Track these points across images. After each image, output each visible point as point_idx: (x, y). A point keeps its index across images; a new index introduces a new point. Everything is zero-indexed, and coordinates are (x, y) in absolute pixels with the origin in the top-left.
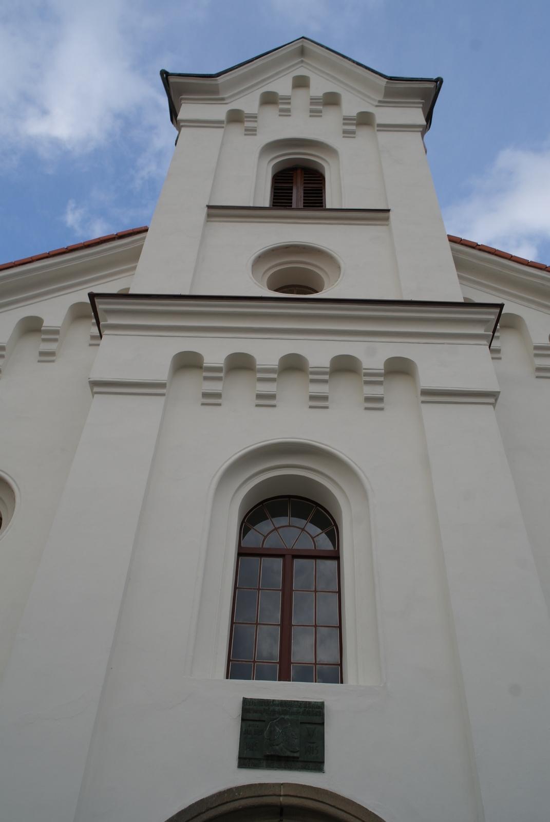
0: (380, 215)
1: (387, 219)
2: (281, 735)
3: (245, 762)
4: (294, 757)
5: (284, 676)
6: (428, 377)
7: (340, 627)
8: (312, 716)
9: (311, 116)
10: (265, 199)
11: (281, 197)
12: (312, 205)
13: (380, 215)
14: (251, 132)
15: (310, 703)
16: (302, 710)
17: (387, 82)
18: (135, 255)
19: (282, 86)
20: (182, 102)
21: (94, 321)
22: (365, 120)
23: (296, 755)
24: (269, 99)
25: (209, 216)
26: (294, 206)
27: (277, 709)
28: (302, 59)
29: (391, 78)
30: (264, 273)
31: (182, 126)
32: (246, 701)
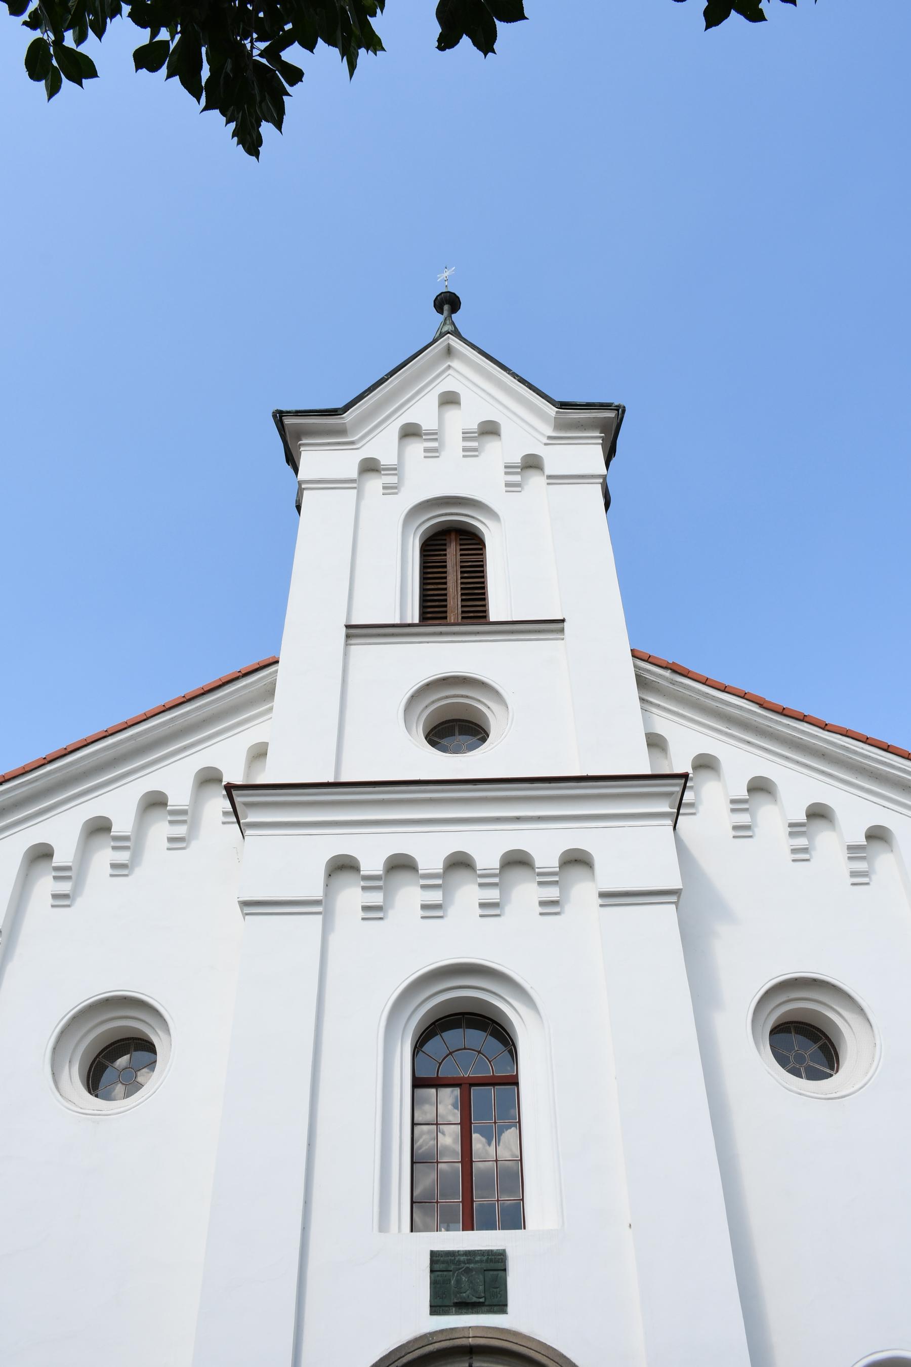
1: (562, 631)
2: (466, 1282)
3: (436, 1309)
5: (468, 1225)
6: (610, 874)
7: (521, 1160)
8: (494, 1265)
10: (413, 615)
11: (433, 611)
12: (472, 615)
14: (390, 489)
15: (492, 1251)
17: (557, 412)
18: (269, 693)
19: (423, 411)
20: (302, 449)
21: (235, 820)
22: (532, 464)
23: (482, 1300)
24: (410, 432)
25: (348, 636)
26: (452, 618)
27: (462, 1258)
28: (449, 363)
29: (563, 405)
30: (418, 527)
32: (433, 1253)
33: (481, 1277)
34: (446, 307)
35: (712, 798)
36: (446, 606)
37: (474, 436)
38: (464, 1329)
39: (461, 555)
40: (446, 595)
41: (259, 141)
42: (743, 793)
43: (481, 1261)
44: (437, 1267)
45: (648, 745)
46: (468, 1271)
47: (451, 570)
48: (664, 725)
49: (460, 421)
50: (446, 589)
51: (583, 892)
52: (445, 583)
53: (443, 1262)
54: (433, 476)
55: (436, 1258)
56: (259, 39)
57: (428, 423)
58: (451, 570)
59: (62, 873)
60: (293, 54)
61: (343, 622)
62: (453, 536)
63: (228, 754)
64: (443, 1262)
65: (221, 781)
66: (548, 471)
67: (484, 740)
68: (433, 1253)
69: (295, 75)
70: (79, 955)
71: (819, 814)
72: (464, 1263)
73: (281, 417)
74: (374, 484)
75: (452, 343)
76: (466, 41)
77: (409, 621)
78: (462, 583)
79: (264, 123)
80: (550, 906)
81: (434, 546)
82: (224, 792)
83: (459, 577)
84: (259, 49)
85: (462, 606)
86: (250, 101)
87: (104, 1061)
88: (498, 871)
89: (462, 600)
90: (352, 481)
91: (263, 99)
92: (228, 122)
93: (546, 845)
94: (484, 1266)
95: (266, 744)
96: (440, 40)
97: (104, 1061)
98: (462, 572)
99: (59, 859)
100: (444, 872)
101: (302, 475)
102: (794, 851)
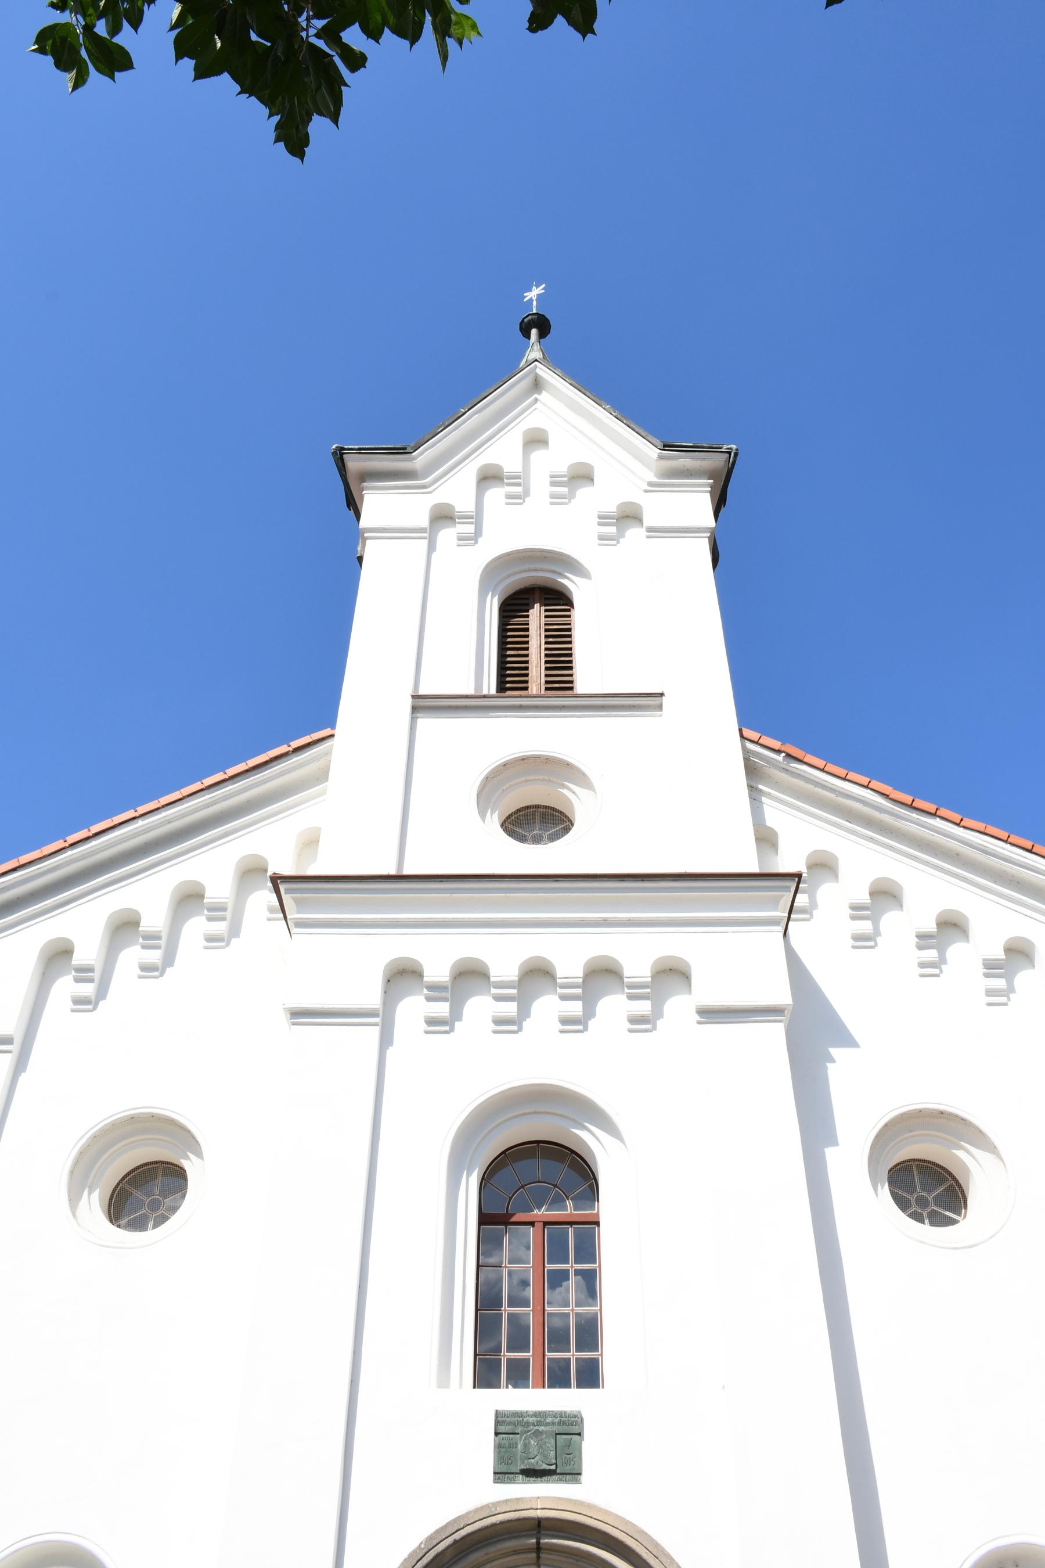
0: (648, 701)
1: (660, 707)
2: (538, 1450)
3: (501, 1475)
4: (550, 1470)
6: (708, 989)
8: (568, 1428)
9: (552, 504)
10: (490, 685)
13: (648, 701)
16: (557, 1420)
21: (282, 916)
22: (629, 516)
23: (553, 1467)
24: (489, 477)
25: (415, 709)
27: (531, 1420)
28: (536, 396)
31: (367, 538)
33: (553, 1441)
34: (534, 332)
35: (832, 902)
36: (527, 675)
37: (565, 471)
38: (531, 1499)
39: (546, 617)
40: (527, 662)
41: (305, 141)
42: (865, 898)
43: (553, 1424)
44: (502, 1429)
45: (756, 839)
46: (538, 1433)
47: (532, 603)
48: (777, 815)
49: (546, 464)
50: (527, 656)
51: (680, 1008)
52: (527, 649)
53: (509, 1423)
54: (516, 527)
55: (500, 1418)
56: (318, 16)
57: (511, 464)
58: (532, 603)
59: (84, 973)
60: (353, 36)
61: (409, 691)
62: (537, 594)
63: (273, 842)
64: (509, 1423)
65: (266, 871)
66: (648, 521)
67: (567, 829)
68: (497, 1414)
69: (356, 61)
70: (98, 1071)
71: (952, 926)
72: (533, 1424)
73: (342, 454)
74: (447, 536)
75: (538, 371)
76: (560, 21)
77: (485, 692)
78: (546, 649)
79: (316, 118)
80: (640, 1022)
81: (513, 607)
82: (270, 884)
83: (543, 655)
84: (315, 28)
85: (546, 676)
86: (298, 91)
87: (127, 1187)
88: (581, 980)
89: (547, 669)
90: (422, 530)
91: (319, 87)
92: (271, 115)
93: (637, 952)
94: (557, 1429)
95: (318, 830)
96: (531, 20)
97: (127, 1187)
98: (546, 637)
99: (79, 958)
100: (520, 980)
101: (364, 523)
102: (922, 965)
